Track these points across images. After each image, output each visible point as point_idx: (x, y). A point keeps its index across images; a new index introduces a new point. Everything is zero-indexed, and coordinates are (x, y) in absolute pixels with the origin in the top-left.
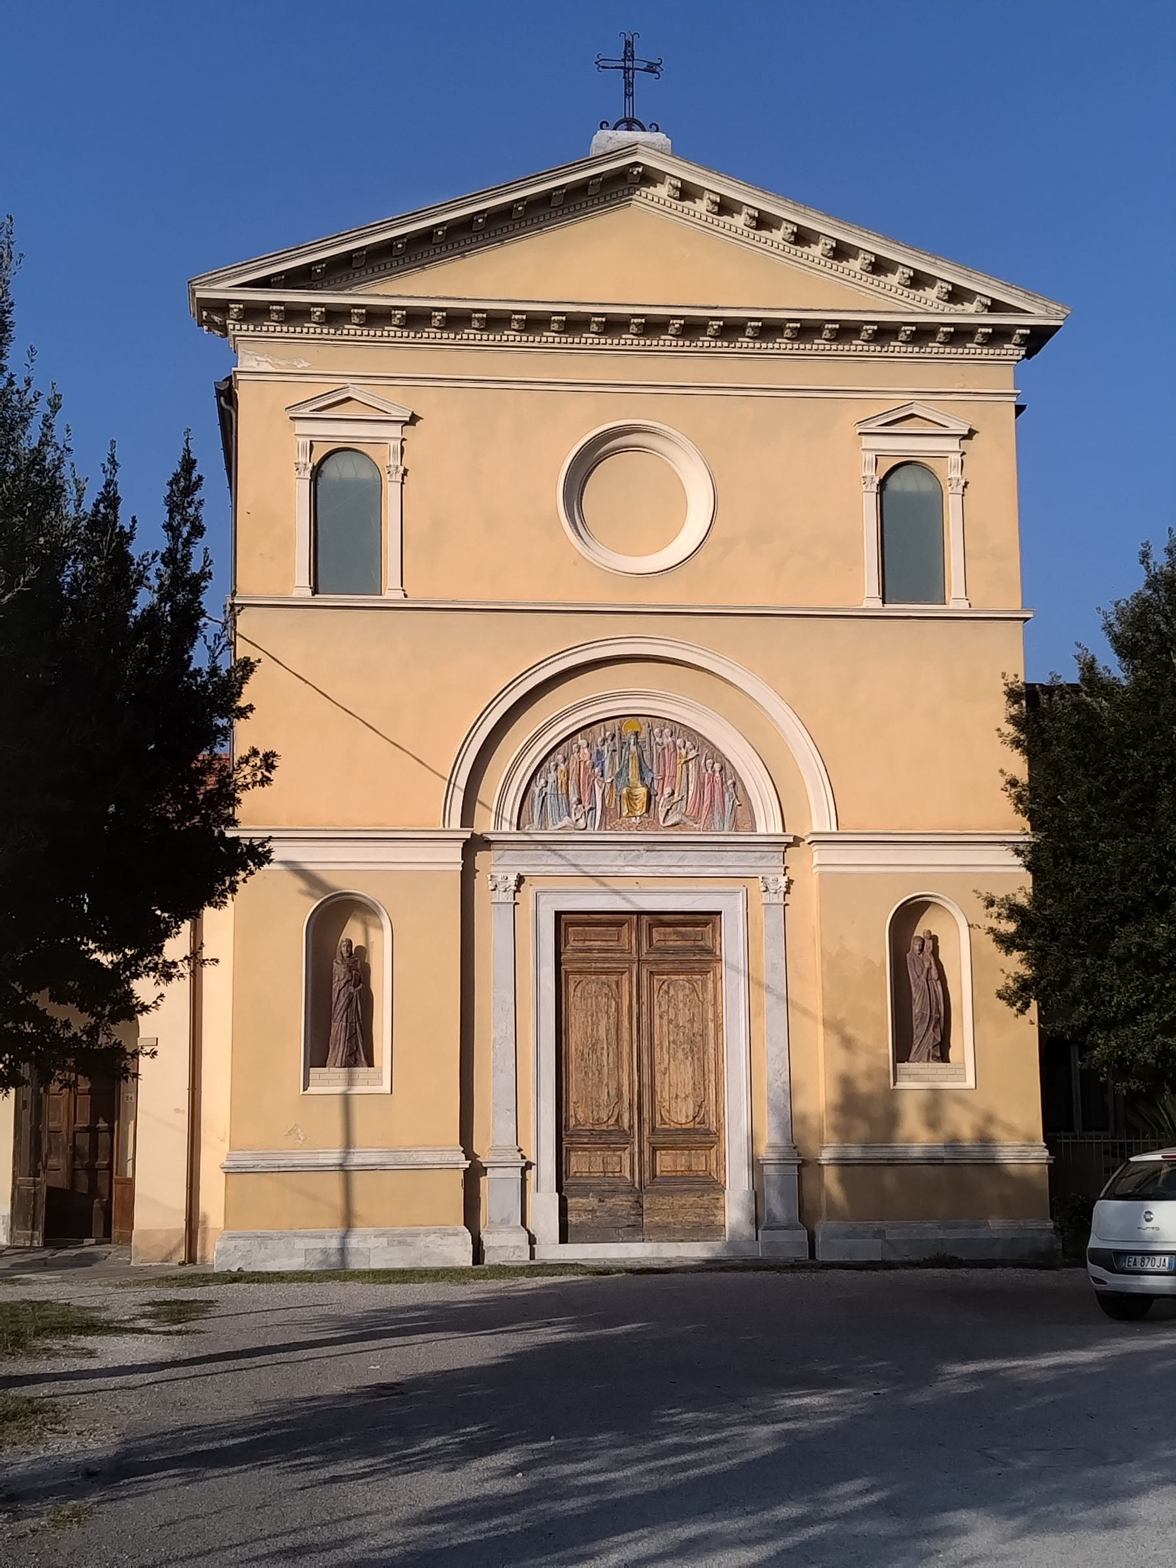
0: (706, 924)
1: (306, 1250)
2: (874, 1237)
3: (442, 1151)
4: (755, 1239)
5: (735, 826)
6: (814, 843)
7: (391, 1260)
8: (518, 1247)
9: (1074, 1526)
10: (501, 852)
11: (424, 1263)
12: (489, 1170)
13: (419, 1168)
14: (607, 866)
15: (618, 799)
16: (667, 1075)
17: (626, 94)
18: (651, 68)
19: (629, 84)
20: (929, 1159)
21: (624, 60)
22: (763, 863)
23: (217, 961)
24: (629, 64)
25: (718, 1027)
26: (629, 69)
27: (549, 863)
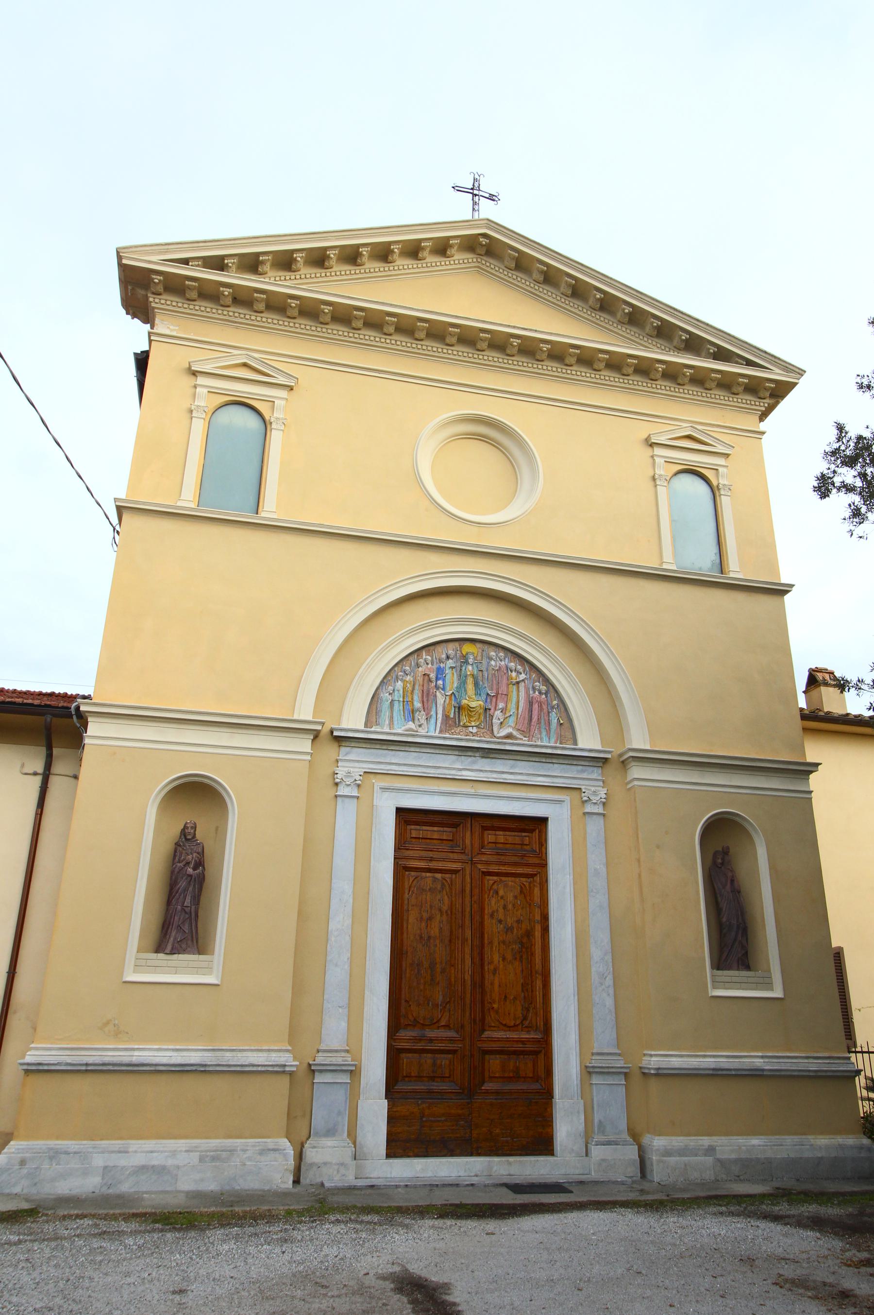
0: (532, 831)
1: (105, 1168)
2: (706, 1155)
3: (269, 1050)
4: (584, 1154)
5: (561, 739)
6: (631, 759)
7: (202, 1180)
8: (342, 1164)
9: (260, 1190)
10: (349, 748)
11: (239, 1185)
12: (316, 1074)
13: (434, 1092)
14: (446, 768)
15: (457, 710)
16: (497, 975)
17: (474, 209)
18: (492, 198)
19: (475, 203)
20: (714, 1069)
21: (472, 189)
22: (585, 775)
23: (292, 389)
24: (476, 192)
25: (546, 930)
26: (476, 195)
27: (393, 761)
